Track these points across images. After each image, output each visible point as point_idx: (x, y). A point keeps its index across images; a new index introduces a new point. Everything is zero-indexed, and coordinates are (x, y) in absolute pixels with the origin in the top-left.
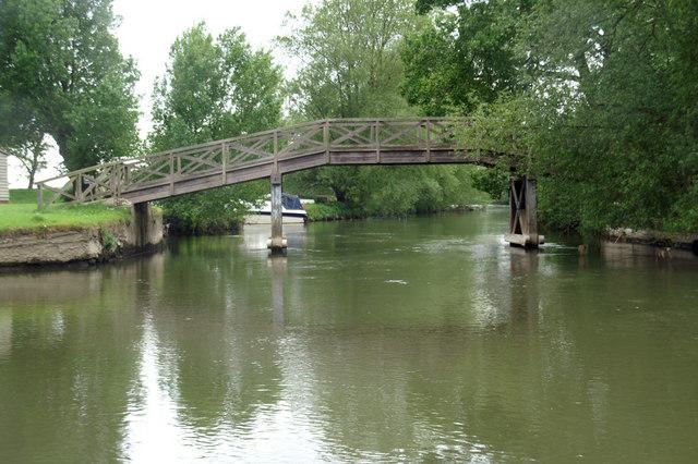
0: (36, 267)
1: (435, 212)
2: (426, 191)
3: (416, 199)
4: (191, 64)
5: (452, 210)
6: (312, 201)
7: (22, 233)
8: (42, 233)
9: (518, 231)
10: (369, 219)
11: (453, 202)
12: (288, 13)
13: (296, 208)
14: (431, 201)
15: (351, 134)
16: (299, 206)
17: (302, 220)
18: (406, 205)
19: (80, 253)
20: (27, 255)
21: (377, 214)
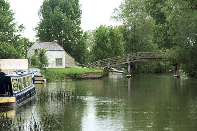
0: (93, 78)
1: (163, 72)
2: (159, 65)
3: (156, 67)
4: (102, 36)
5: (169, 72)
6: (124, 68)
7: (92, 73)
8: (94, 73)
9: (176, 74)
10: (141, 74)
11: (170, 69)
12: (116, 9)
13: (120, 70)
14: (161, 68)
15: (143, 55)
16: (121, 70)
17: (122, 73)
18: (152, 70)
19: (99, 76)
20: (92, 76)
21: (143, 72)
